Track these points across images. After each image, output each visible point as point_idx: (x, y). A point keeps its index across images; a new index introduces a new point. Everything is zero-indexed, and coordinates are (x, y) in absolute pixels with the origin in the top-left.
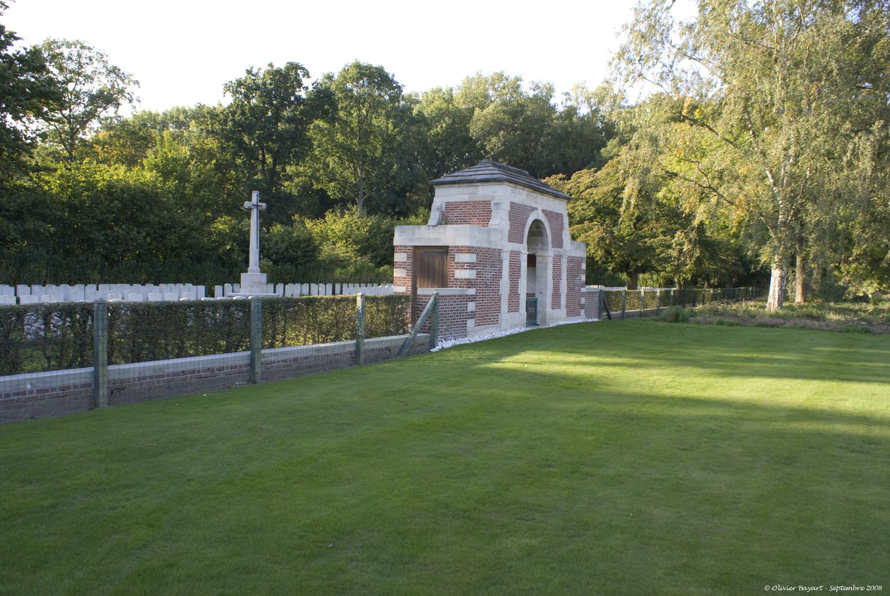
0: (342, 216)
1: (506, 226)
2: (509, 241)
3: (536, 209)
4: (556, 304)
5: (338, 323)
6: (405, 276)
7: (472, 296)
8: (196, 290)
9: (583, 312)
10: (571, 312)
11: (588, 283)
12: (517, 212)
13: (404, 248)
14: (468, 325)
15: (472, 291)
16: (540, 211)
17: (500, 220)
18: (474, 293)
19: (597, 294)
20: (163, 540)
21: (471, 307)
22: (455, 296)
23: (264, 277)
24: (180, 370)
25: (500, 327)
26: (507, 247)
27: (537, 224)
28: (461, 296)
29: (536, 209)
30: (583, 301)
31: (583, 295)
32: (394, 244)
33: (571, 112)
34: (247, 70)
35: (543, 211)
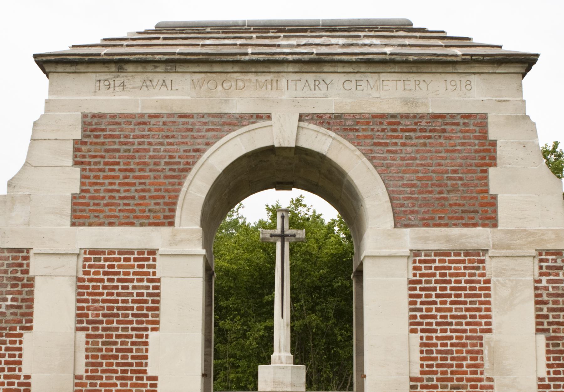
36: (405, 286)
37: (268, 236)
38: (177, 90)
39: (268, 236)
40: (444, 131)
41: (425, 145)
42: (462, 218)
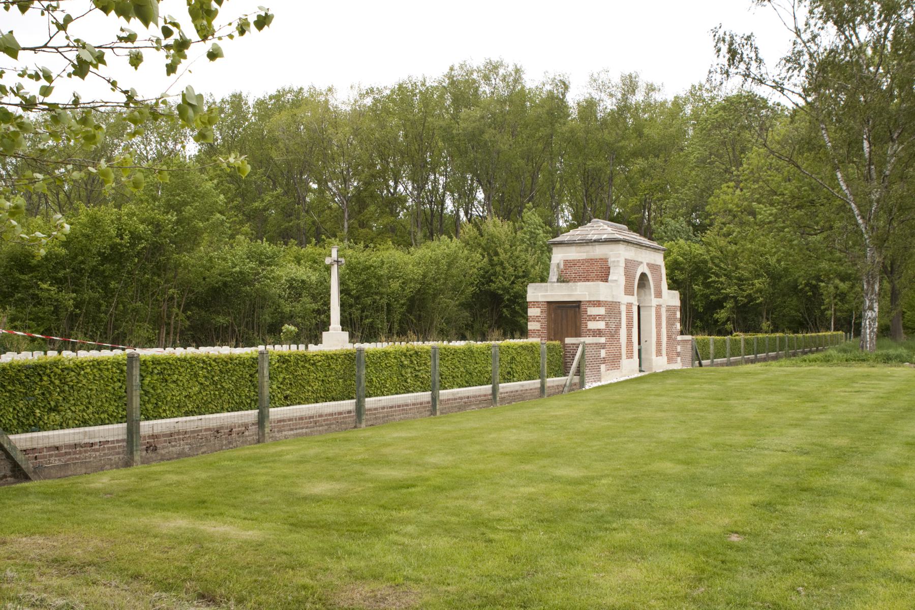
1: (622, 281)
3: (642, 263)
4: (659, 353)
6: (539, 328)
9: (679, 359)
10: (670, 360)
11: (682, 333)
12: (630, 266)
13: (536, 304)
15: (602, 340)
16: (645, 264)
17: (618, 275)
19: (690, 342)
21: (603, 353)
23: (346, 335)
24: (418, 401)
25: (621, 372)
26: (625, 299)
27: (643, 276)
29: (642, 263)
30: (679, 349)
31: (679, 342)
32: (528, 300)
33: (589, 107)
34: (104, 63)
35: (648, 264)
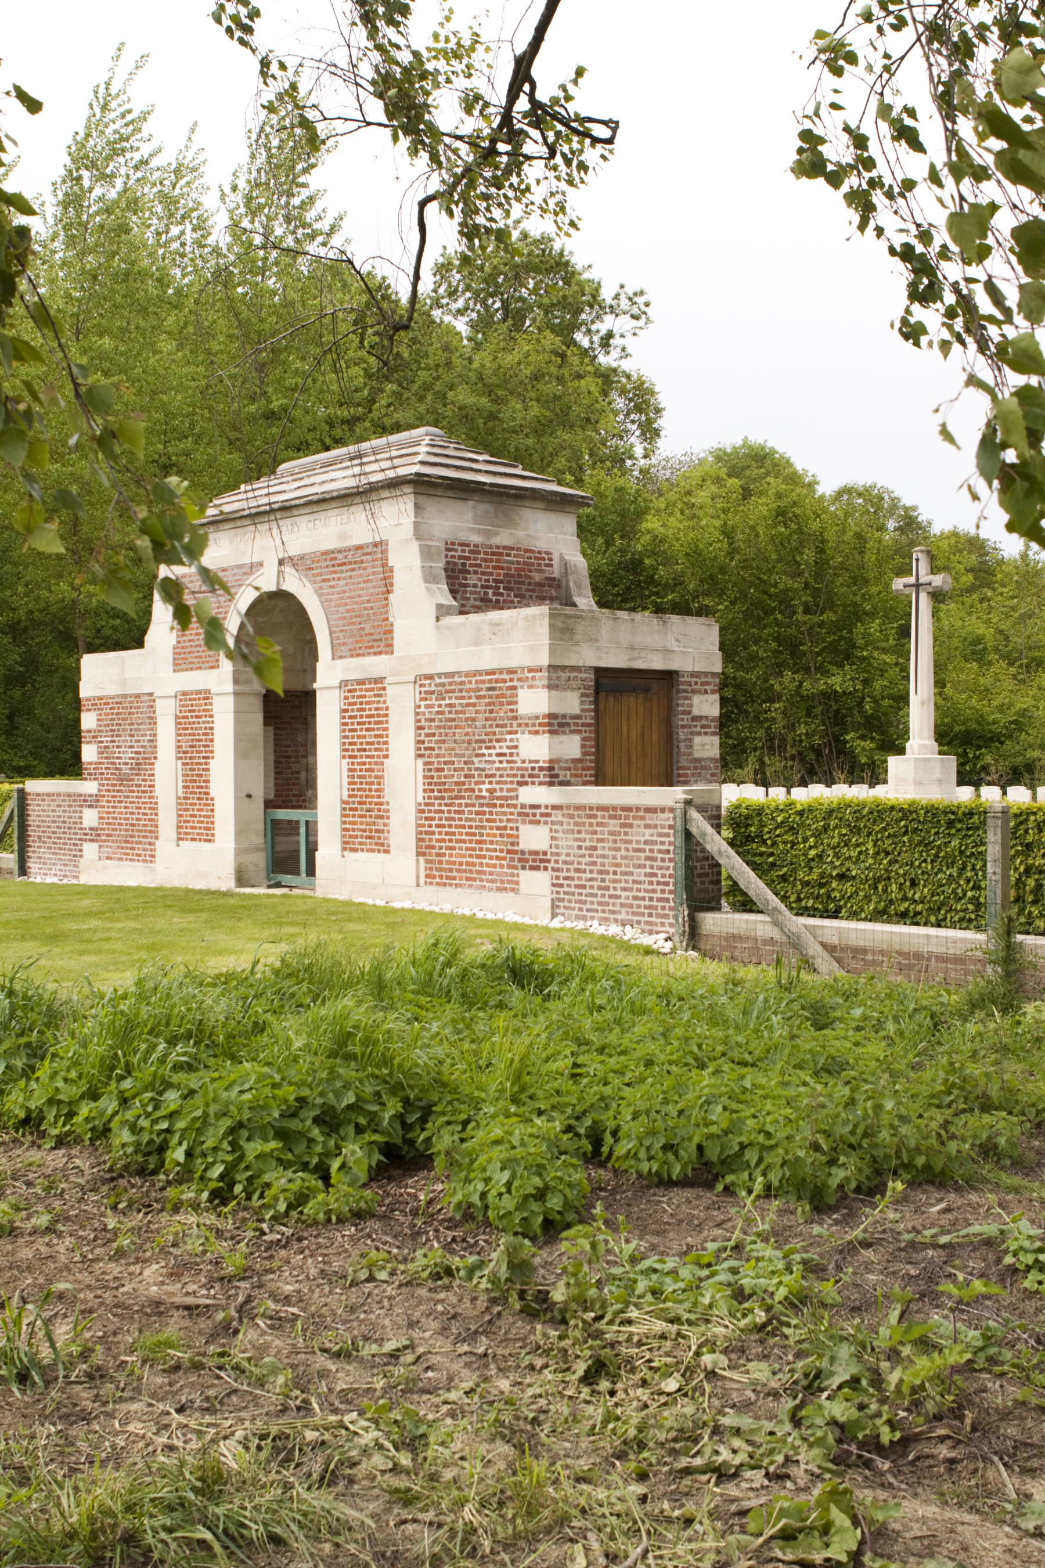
0: (820, 1292)
2: (139, 644)
5: (468, 1027)
7: (91, 796)
8: (325, 692)
14: (84, 853)
18: (95, 791)
20: (200, 1479)
22: (59, 795)
28: (69, 795)
36: (337, 714)
37: (901, 587)
38: (937, 411)
39: (901, 587)
40: (362, 562)
41: (351, 577)
42: (372, 647)
